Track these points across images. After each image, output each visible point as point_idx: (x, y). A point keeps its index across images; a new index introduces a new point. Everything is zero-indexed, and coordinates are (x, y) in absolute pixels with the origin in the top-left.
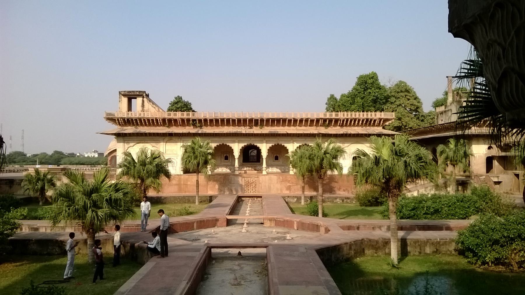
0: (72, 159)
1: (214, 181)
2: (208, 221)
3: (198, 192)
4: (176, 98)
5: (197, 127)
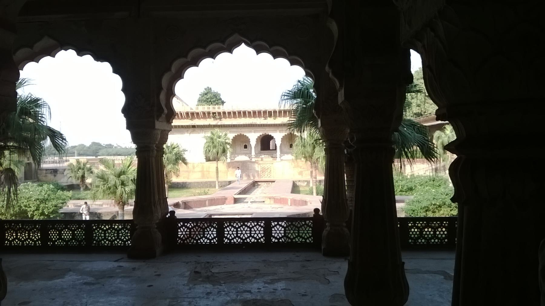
0: (110, 150)
2: (218, 199)
3: (218, 177)
4: (206, 89)
5: (217, 119)
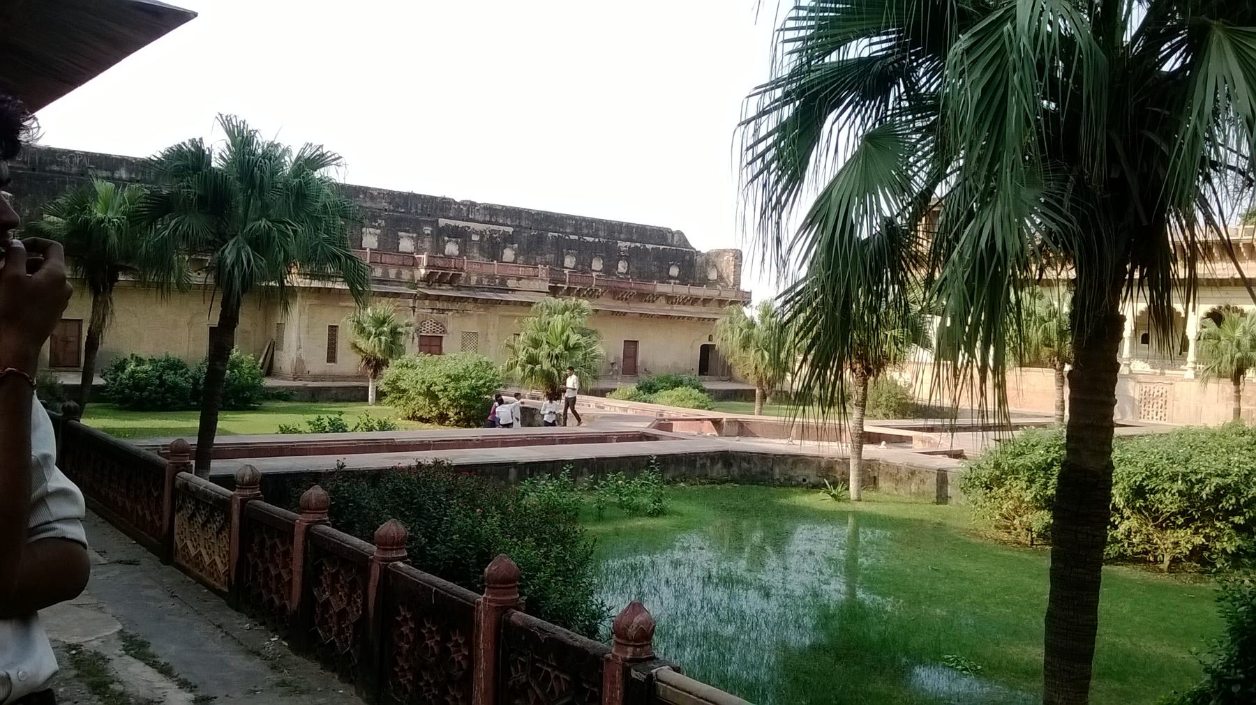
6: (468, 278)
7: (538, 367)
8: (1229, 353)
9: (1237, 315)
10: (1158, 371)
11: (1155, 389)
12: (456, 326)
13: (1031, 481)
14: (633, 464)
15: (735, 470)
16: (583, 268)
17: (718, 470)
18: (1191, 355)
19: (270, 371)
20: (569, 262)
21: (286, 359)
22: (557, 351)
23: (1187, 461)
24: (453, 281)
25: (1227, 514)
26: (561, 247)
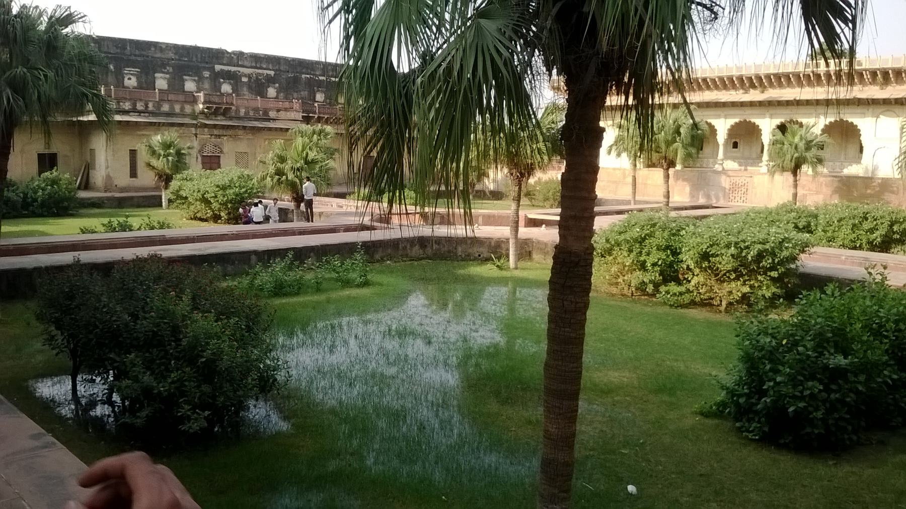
1: (684, 180)
3: (634, 193)
6: (237, 111)
7: (284, 177)
8: (790, 155)
9: (797, 126)
10: (743, 168)
11: (740, 181)
12: (230, 148)
13: (630, 251)
14: (351, 249)
15: (429, 251)
16: (331, 101)
17: (416, 251)
18: (765, 157)
19: (86, 185)
20: (320, 97)
21: (99, 176)
22: (299, 165)
23: (739, 232)
24: (226, 113)
25: (767, 270)
26: (313, 86)
